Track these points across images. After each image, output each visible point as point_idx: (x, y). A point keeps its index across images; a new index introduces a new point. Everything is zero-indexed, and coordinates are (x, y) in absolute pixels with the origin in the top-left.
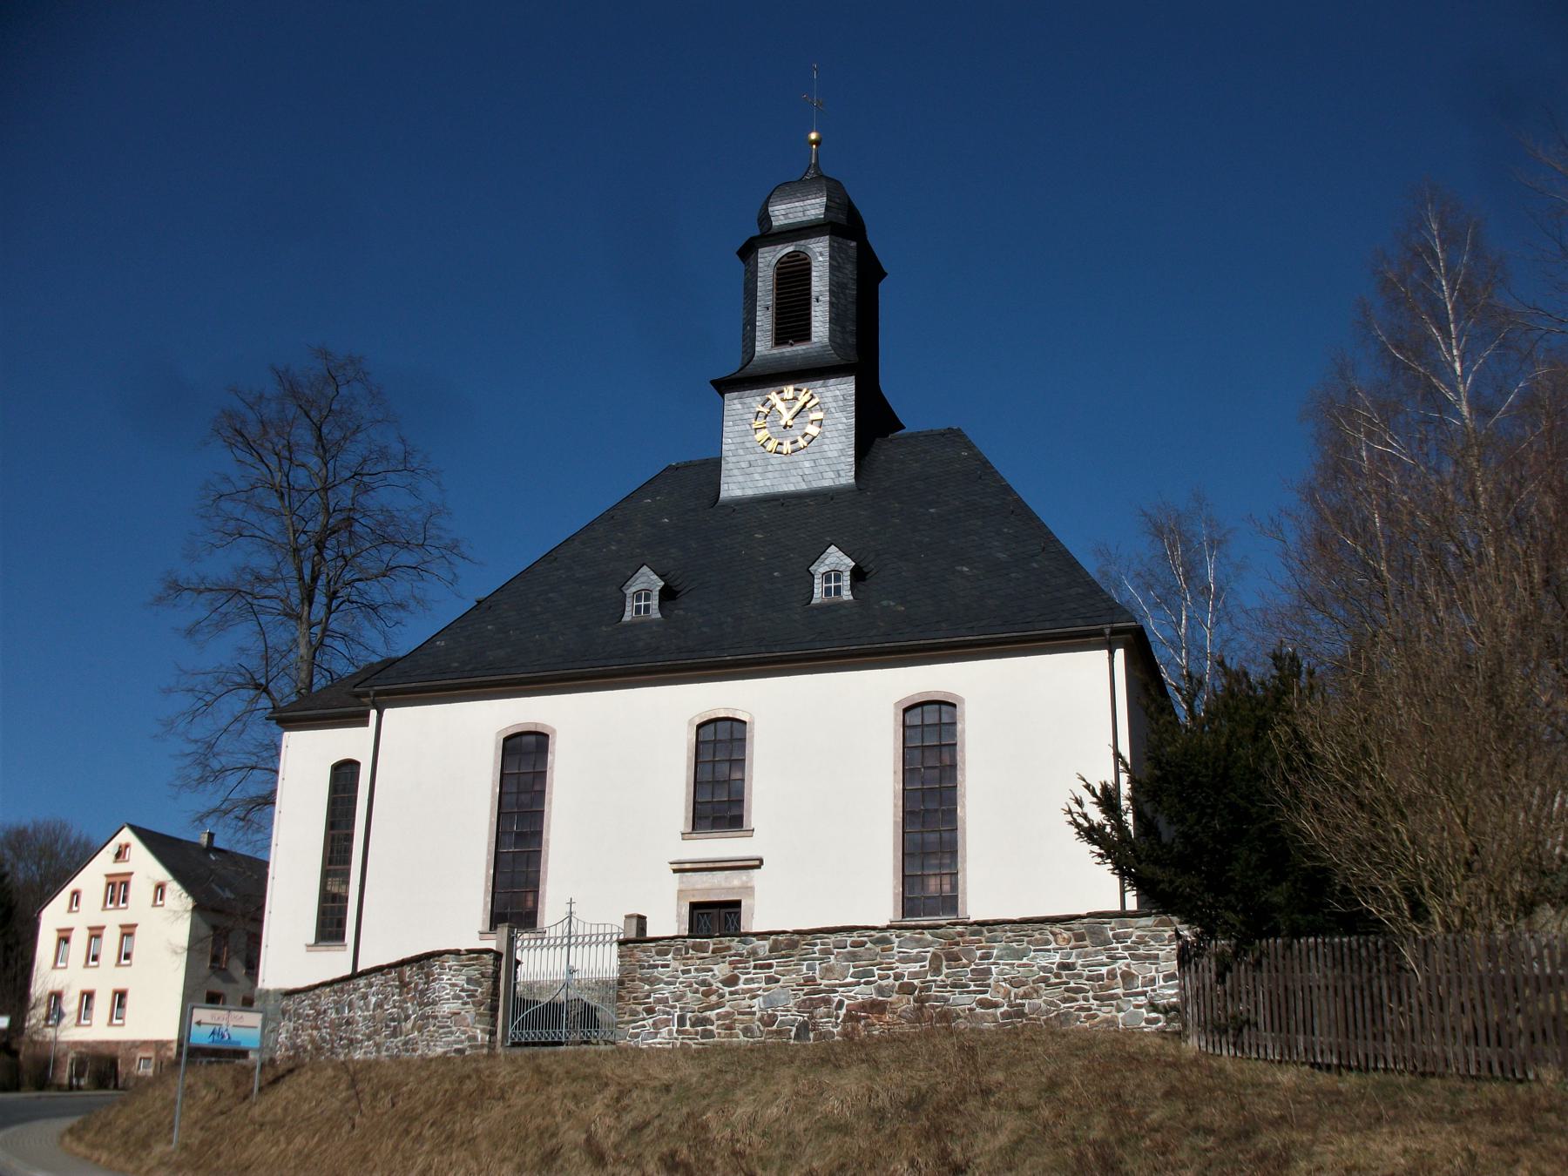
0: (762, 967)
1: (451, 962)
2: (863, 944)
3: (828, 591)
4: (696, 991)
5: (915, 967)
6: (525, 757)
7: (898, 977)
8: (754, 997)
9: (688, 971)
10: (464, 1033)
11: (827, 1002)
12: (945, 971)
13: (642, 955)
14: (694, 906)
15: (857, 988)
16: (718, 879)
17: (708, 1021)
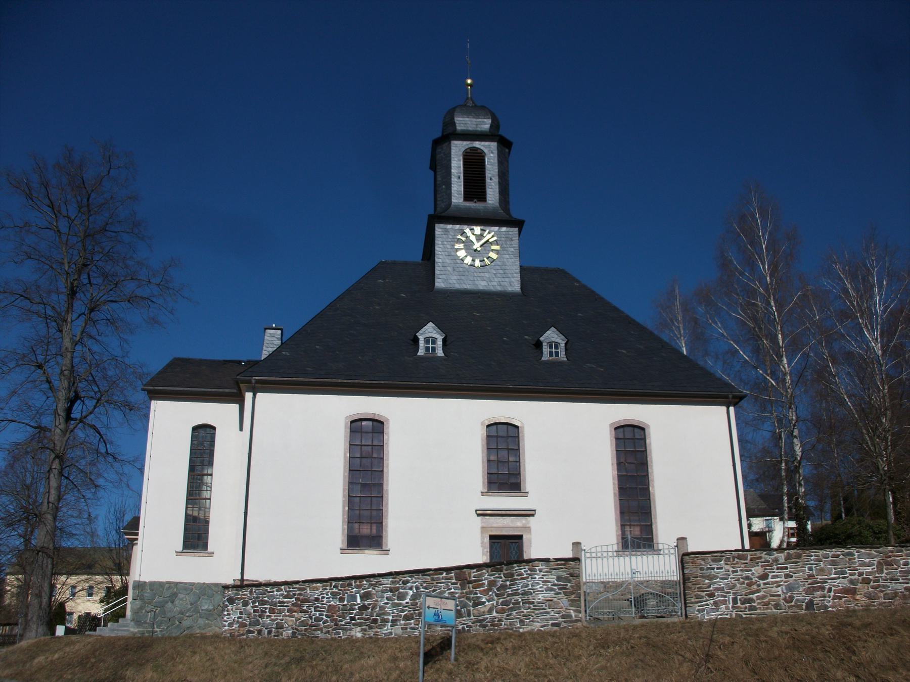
0: (782, 568)
1: (540, 566)
2: (838, 556)
3: (551, 353)
4: (743, 583)
5: (869, 569)
6: (367, 439)
7: (860, 574)
8: (779, 586)
9: (737, 571)
10: (559, 613)
11: (823, 588)
12: (885, 571)
13: (702, 563)
14: (492, 537)
15: (838, 581)
16: (507, 521)
17: (751, 601)
